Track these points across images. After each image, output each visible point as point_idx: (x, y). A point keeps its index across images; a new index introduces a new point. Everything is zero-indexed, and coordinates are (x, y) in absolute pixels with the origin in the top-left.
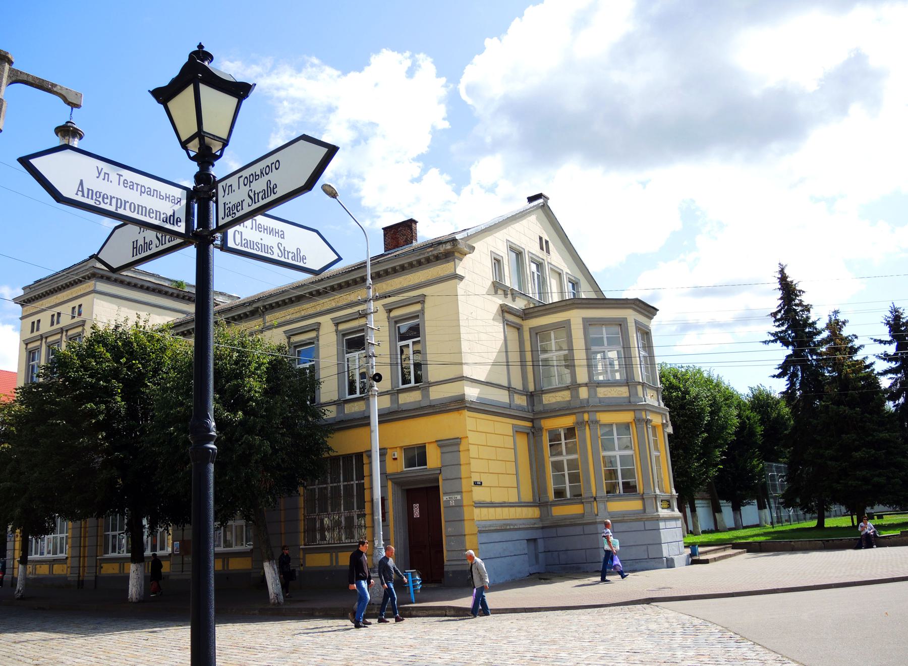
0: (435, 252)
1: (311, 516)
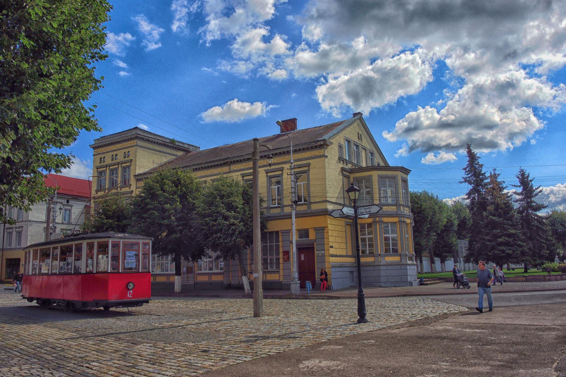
0: (315, 145)
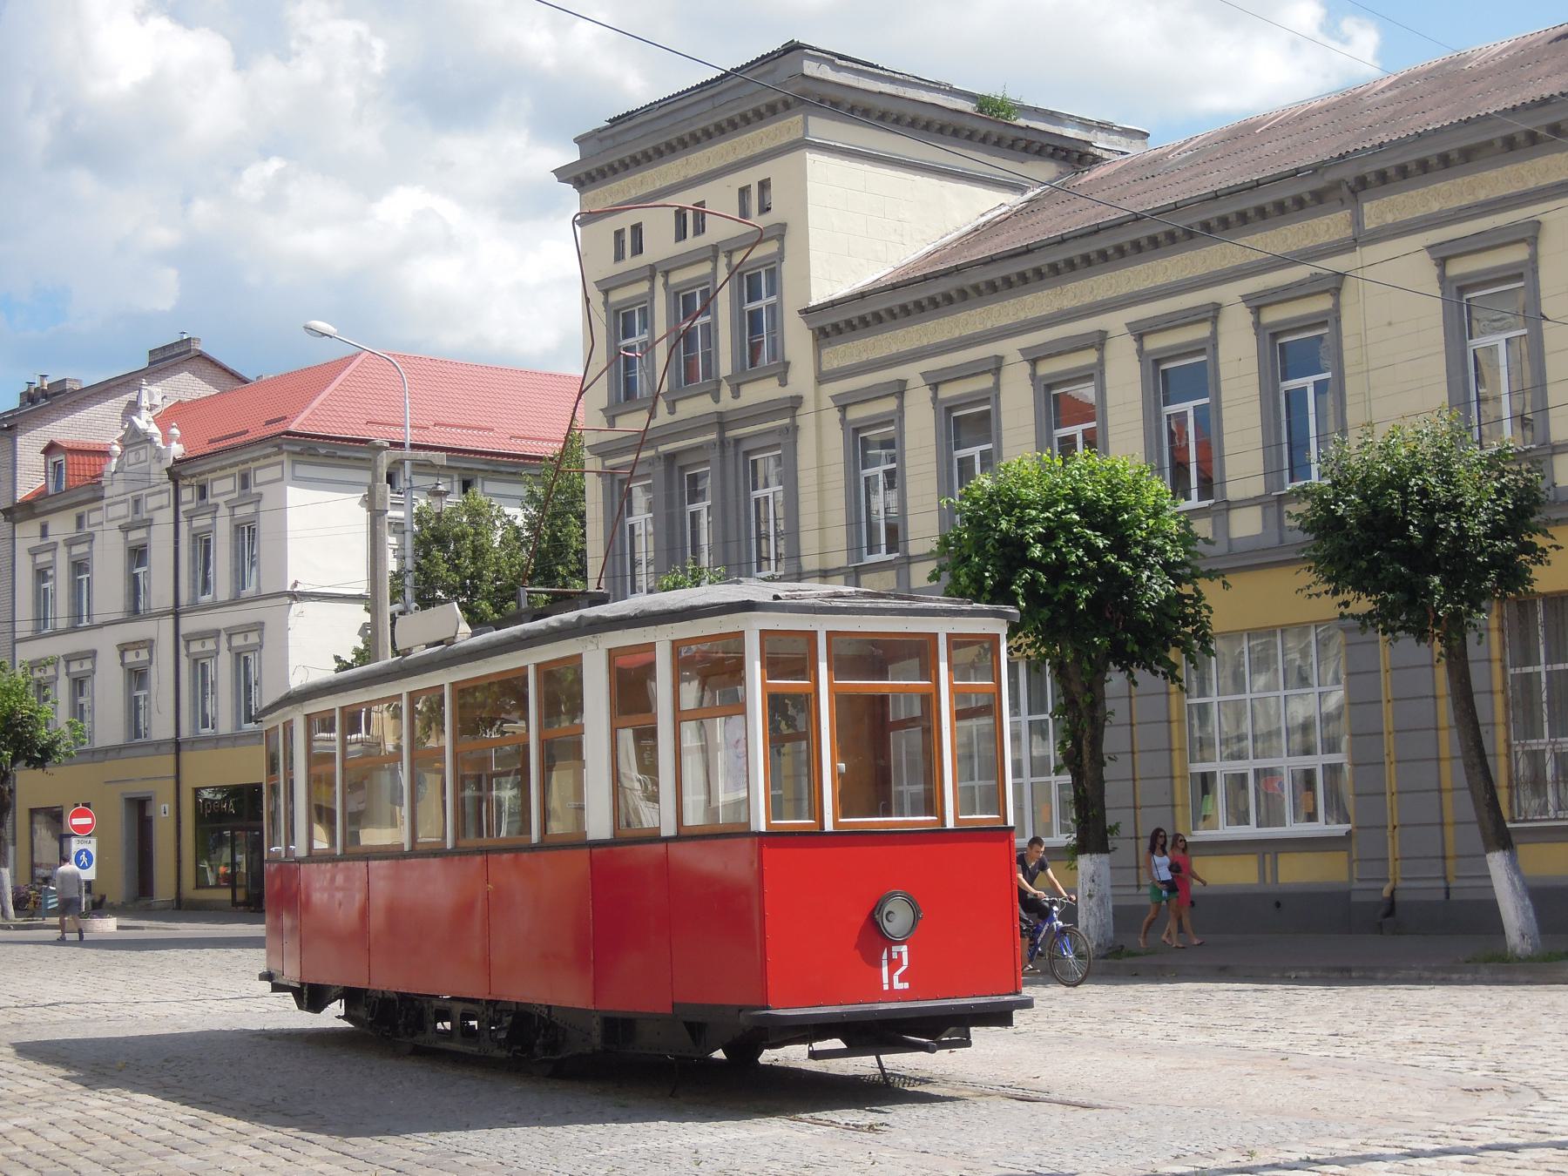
1: (1529, 745)
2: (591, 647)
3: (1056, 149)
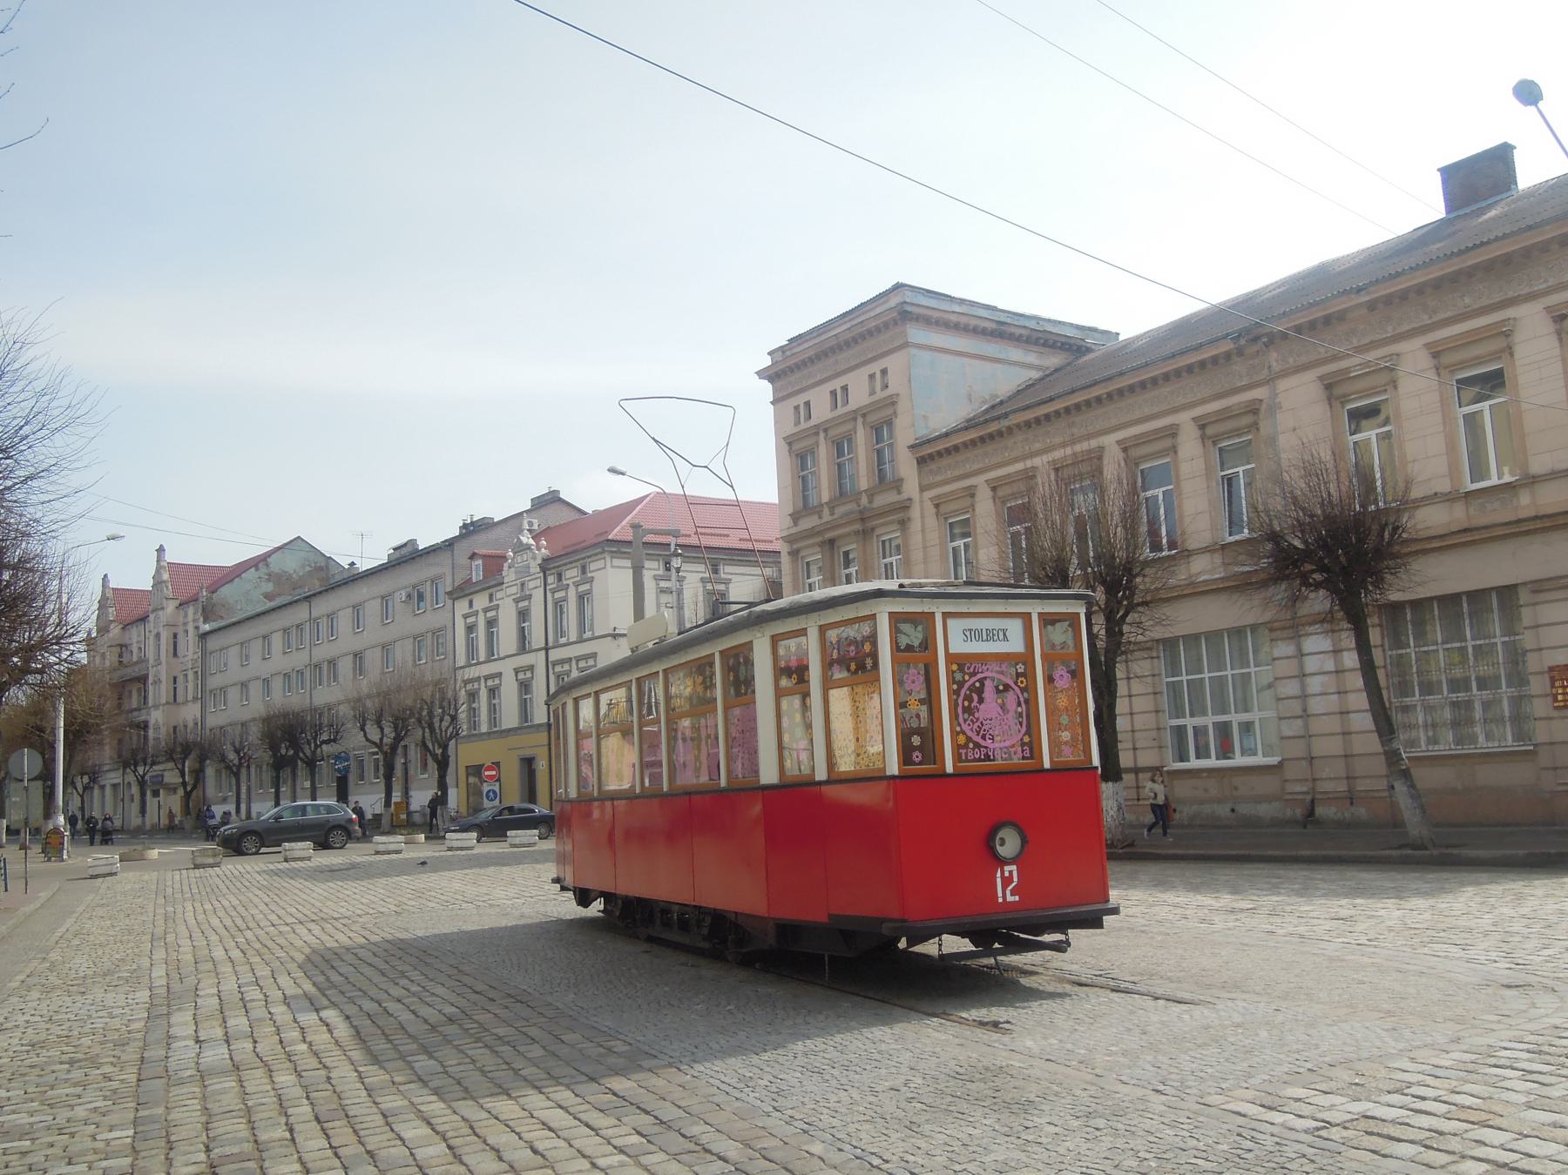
2: (759, 635)
3: (1063, 344)
